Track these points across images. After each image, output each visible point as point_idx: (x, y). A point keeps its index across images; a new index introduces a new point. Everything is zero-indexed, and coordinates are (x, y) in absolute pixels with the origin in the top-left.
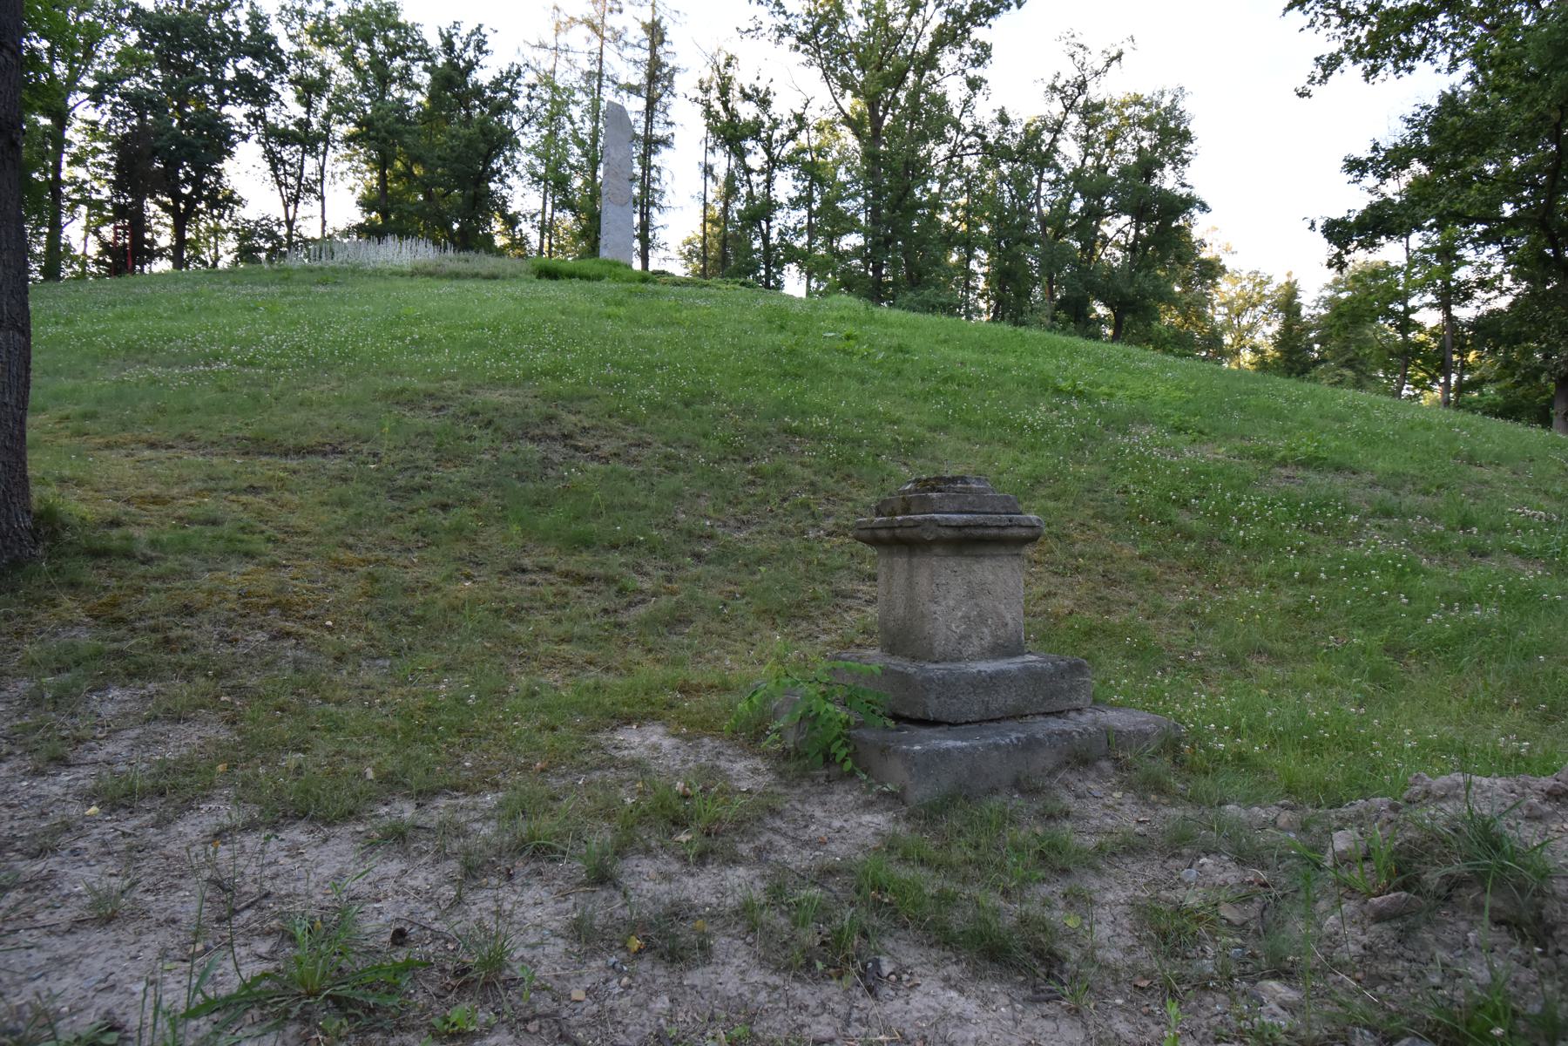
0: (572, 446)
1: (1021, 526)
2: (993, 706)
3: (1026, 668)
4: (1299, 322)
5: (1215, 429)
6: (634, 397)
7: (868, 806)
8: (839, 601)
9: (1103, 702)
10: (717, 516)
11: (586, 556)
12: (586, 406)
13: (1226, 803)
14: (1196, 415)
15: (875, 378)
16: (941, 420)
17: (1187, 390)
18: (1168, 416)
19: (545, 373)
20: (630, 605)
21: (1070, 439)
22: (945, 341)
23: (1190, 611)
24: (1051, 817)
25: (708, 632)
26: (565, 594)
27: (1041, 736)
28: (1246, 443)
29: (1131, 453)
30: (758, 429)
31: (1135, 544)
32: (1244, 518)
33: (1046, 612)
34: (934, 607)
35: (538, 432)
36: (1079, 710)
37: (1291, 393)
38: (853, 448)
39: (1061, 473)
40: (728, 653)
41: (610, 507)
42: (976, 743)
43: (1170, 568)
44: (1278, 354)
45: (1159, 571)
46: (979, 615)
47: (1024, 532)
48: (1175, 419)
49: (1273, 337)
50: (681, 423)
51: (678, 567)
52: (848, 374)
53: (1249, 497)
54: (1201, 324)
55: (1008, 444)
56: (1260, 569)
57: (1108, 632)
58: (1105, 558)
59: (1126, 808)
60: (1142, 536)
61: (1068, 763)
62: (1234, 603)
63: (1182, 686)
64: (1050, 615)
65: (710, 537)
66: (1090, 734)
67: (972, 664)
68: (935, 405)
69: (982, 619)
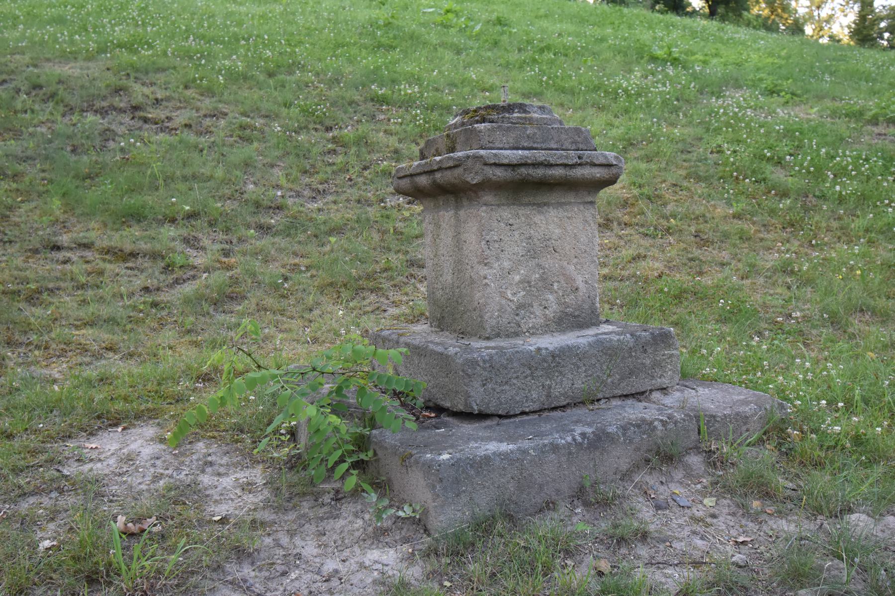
0: (140, 118)
1: (595, 165)
2: (557, 391)
3: (599, 342)
4: (873, 11)
5: (807, 91)
6: (213, 69)
7: (378, 536)
8: (415, 271)
9: (693, 376)
10: (290, 185)
11: (136, 231)
12: (161, 78)
13: (850, 511)
14: (788, 79)
15: (472, 48)
16: (535, 87)
17: (779, 57)
18: (761, 80)
19: (120, 46)
20: (177, 282)
21: (665, 103)
22: (546, 16)
23: (786, 269)
24: (622, 541)
25: (261, 309)
26: (101, 273)
27: (612, 429)
28: (837, 104)
29: (725, 114)
30: (343, 98)
31: (729, 204)
32: (840, 173)
33: (634, 275)
34: (484, 271)
35: (105, 104)
36: (663, 390)
37: (877, 60)
38: (441, 115)
39: (654, 135)
40: (281, 331)
41: (169, 179)
42: (526, 444)
43: (764, 226)
44: (852, 43)
45: (753, 228)
46: (543, 279)
47: (598, 173)
48: (768, 82)
49: (849, 27)
50: (262, 92)
51: (240, 240)
52: (443, 45)
53: (844, 153)
54: (786, 16)
55: (601, 109)
56: (857, 224)
57: (698, 295)
58: (697, 218)
59: (720, 523)
60: (736, 195)
61: (648, 461)
62: (832, 259)
63: (782, 351)
64: (637, 278)
65: (279, 208)
66: (676, 423)
67: (533, 340)
68: (529, 73)
69: (546, 283)
